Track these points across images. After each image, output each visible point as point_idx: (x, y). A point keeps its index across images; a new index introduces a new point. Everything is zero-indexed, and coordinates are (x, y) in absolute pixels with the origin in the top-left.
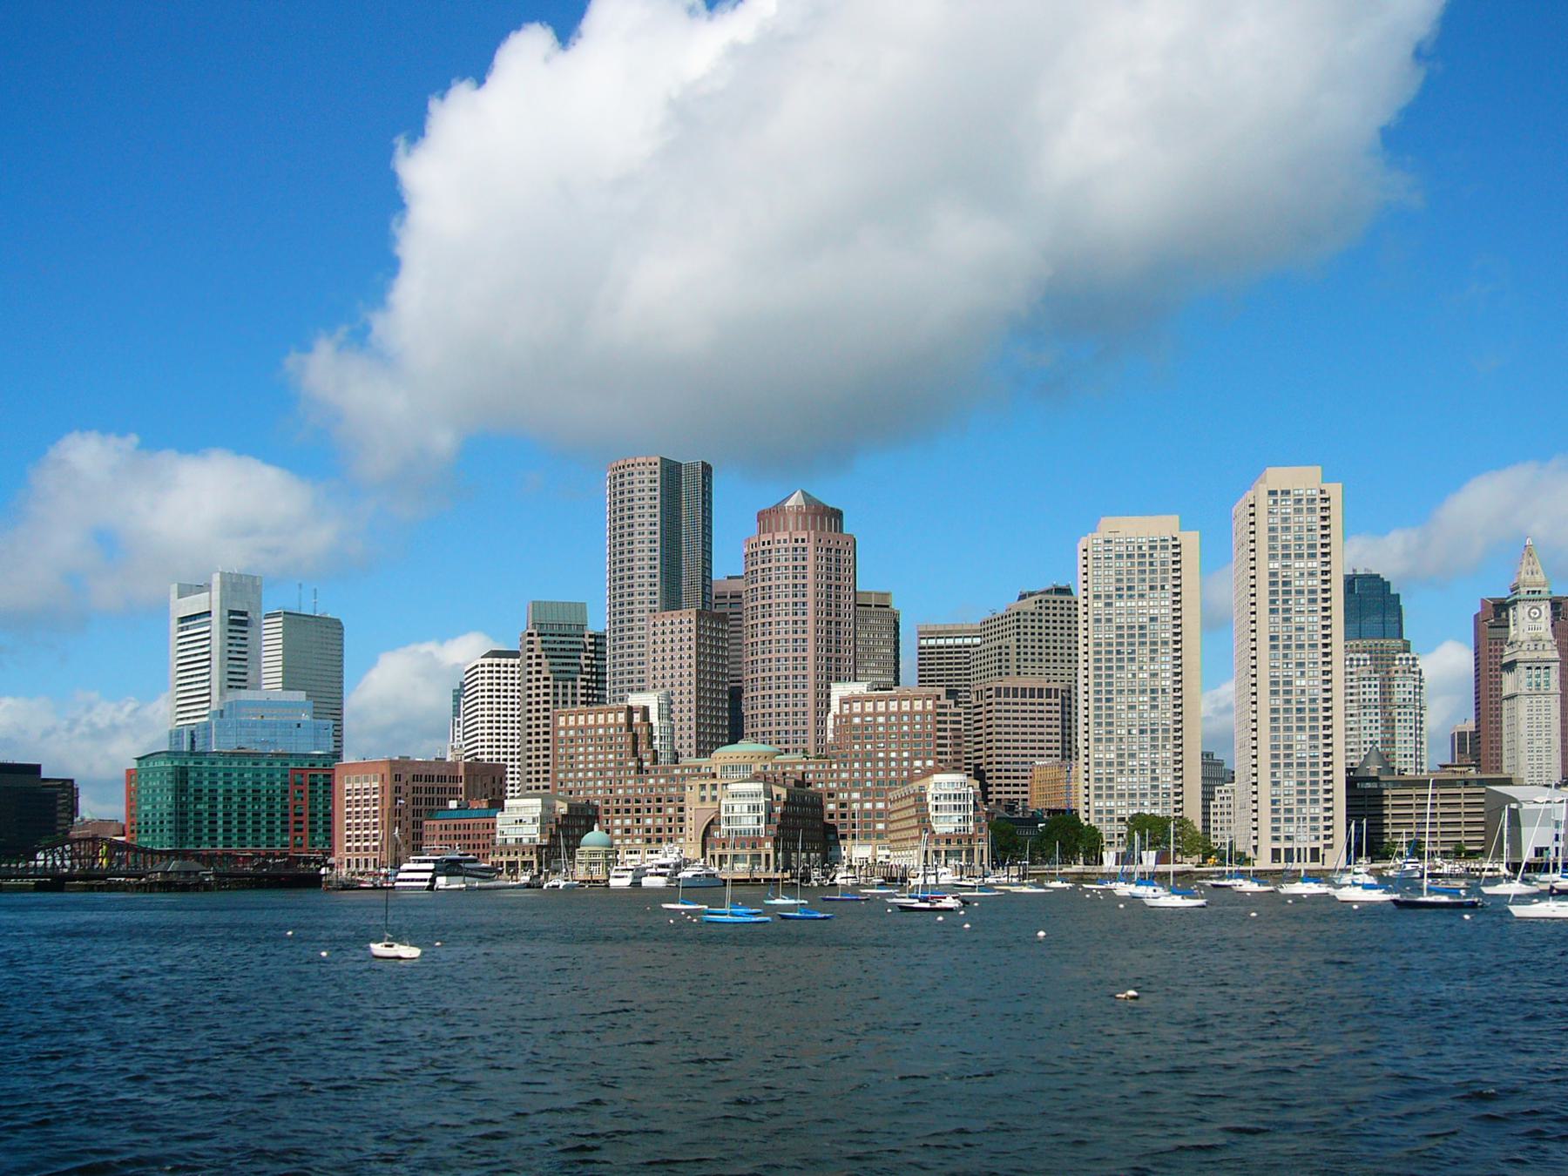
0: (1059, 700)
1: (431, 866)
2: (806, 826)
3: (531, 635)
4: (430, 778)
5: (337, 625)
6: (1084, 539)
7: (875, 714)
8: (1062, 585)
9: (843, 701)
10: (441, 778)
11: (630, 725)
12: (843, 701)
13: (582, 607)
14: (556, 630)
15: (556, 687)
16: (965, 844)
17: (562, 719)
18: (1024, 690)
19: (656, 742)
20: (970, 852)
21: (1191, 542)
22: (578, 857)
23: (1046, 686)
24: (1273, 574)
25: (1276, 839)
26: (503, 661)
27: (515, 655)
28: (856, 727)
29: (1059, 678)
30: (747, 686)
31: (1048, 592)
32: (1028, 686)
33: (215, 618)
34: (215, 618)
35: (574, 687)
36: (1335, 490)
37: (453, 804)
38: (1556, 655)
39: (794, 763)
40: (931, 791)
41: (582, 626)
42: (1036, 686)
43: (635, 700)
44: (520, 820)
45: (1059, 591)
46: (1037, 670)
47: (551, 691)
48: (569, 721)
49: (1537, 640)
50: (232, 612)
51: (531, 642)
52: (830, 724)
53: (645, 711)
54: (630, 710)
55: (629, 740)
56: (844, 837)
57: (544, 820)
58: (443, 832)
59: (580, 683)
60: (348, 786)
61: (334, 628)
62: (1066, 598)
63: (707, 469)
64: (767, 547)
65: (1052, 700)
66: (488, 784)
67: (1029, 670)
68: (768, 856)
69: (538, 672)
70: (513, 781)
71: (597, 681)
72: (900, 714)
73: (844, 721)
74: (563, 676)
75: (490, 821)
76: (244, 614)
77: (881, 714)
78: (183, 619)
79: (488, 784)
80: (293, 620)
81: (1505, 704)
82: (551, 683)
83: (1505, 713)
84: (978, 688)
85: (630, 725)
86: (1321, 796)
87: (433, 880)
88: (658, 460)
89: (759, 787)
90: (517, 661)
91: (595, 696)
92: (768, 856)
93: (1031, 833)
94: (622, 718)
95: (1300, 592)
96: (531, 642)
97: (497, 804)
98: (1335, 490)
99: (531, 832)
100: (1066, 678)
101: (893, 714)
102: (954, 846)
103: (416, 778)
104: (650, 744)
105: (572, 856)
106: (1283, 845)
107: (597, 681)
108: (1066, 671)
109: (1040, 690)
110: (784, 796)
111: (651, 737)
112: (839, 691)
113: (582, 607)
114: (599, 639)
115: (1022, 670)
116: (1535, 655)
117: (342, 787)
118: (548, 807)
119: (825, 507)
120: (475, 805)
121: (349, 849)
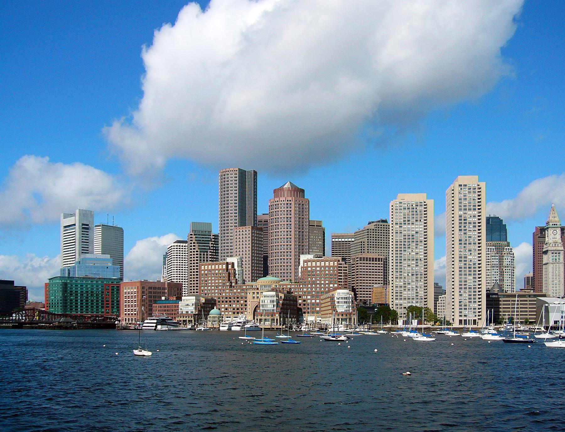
0: (382, 263)
1: (155, 321)
2: (291, 308)
3: (191, 235)
4: (155, 288)
5: (121, 229)
7: (316, 267)
8: (384, 219)
9: (305, 261)
10: (159, 288)
12: (305, 261)
14: (200, 233)
15: (201, 254)
16: (348, 316)
19: (237, 276)
20: (350, 319)
21: (431, 203)
22: (209, 319)
23: (378, 257)
25: (461, 316)
28: (309, 271)
31: (379, 222)
32: (371, 257)
33: (77, 226)
34: (77, 226)
35: (207, 255)
36: (483, 185)
37: (163, 298)
38: (562, 248)
40: (336, 296)
41: (210, 232)
43: (229, 260)
49: (555, 243)
50: (83, 224)
51: (191, 238)
54: (227, 264)
56: (305, 313)
57: (196, 305)
58: (160, 309)
61: (121, 230)
62: (385, 224)
63: (255, 173)
64: (277, 203)
66: (176, 291)
67: (372, 251)
68: (277, 319)
69: (194, 249)
70: (185, 290)
72: (325, 267)
73: (305, 269)
74: (203, 251)
75: (177, 305)
76: (88, 225)
78: (65, 227)
79: (176, 291)
80: (105, 228)
85: (227, 269)
87: (156, 327)
88: (237, 169)
89: (274, 293)
90: (187, 245)
91: (215, 258)
92: (277, 319)
93: (373, 312)
94: (224, 266)
95: (470, 223)
96: (191, 238)
97: (179, 298)
98: (483, 185)
99: (191, 309)
100: (385, 254)
101: (323, 267)
102: (344, 317)
103: (150, 288)
105: (206, 318)
106: (463, 318)
110: (283, 297)
112: (303, 258)
114: (216, 236)
115: (369, 251)
116: (555, 248)
117: (123, 291)
118: (198, 300)
120: (171, 298)
121: (126, 314)
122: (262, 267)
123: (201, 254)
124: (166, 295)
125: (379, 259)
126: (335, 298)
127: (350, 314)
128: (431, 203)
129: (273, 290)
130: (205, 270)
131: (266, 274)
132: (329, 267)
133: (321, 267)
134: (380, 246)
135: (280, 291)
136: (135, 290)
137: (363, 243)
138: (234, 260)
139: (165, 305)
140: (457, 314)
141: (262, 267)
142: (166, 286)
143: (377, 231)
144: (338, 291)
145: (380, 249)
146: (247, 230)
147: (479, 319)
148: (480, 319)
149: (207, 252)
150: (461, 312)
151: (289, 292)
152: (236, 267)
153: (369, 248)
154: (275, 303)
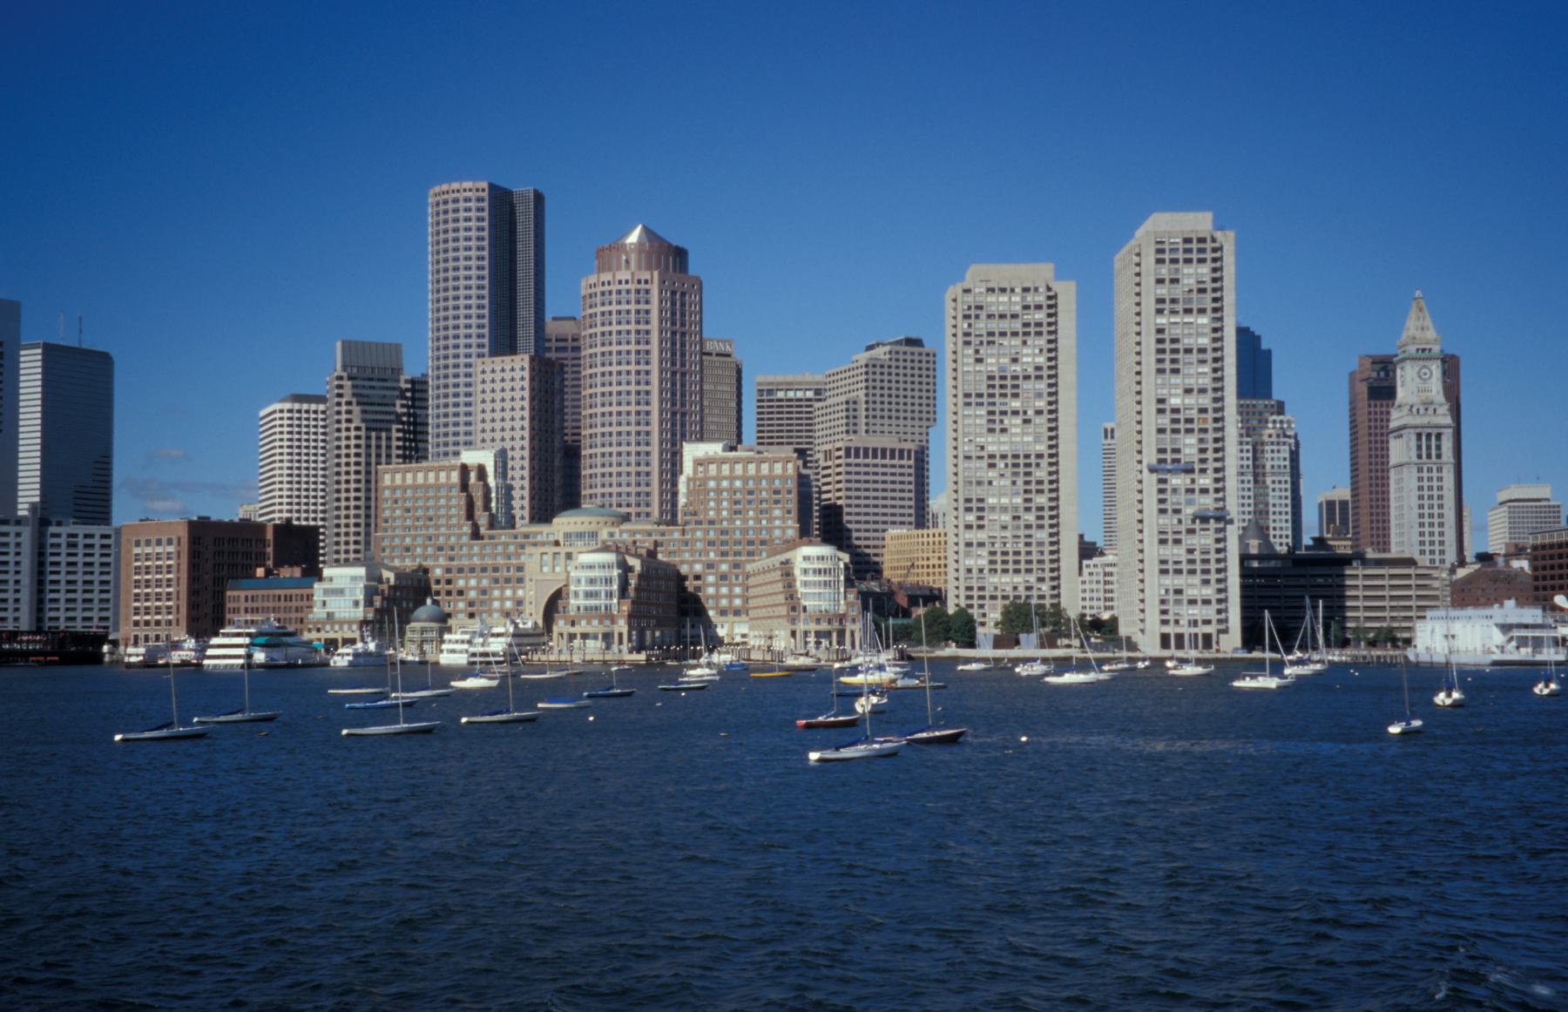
0: (912, 462)
1: (247, 640)
2: (669, 607)
3: (341, 378)
5: (104, 360)
6: (951, 288)
8: (914, 335)
9: (698, 463)
11: (464, 486)
12: (698, 463)
13: (396, 349)
14: (376, 375)
15: (368, 438)
16: (836, 625)
17: (387, 477)
18: (875, 450)
19: (493, 504)
20: (841, 633)
21: (1067, 294)
22: (409, 635)
23: (898, 446)
24: (1160, 331)
25: (1165, 622)
26: (305, 406)
27: (321, 399)
29: (909, 437)
30: (586, 442)
31: (898, 343)
32: (879, 446)
35: (389, 439)
36: (1228, 240)
37: (260, 572)
39: (641, 532)
40: (799, 565)
41: (398, 371)
42: (889, 446)
43: (470, 457)
44: (341, 592)
45: (910, 342)
46: (886, 428)
47: (362, 442)
48: (395, 477)
51: (340, 387)
52: (682, 488)
53: (481, 470)
54: (465, 469)
55: (463, 502)
57: (370, 593)
58: (249, 605)
59: (395, 435)
60: (137, 550)
61: (104, 360)
62: (916, 350)
63: (539, 198)
64: (607, 288)
65: (904, 462)
66: (300, 548)
67: (878, 428)
68: (621, 635)
69: (349, 421)
70: (326, 545)
71: (415, 432)
72: (758, 478)
73: (699, 486)
74: (375, 426)
75: (305, 592)
77: (725, 478)
79: (300, 548)
80: (54, 356)
81: (1393, 475)
82: (362, 433)
83: (1392, 482)
84: (827, 447)
85: (464, 486)
86: (1034, 549)
87: (249, 656)
88: (485, 185)
89: (610, 558)
90: (322, 407)
91: (414, 449)
92: (621, 635)
93: (896, 610)
94: (455, 477)
95: (1188, 351)
96: (340, 387)
97: (313, 573)
98: (1228, 240)
100: (917, 437)
101: (752, 478)
102: (824, 626)
104: (487, 507)
105: (402, 633)
106: (1170, 630)
107: (415, 432)
108: (917, 430)
109: (893, 451)
110: (638, 568)
111: (487, 499)
112: (692, 451)
113: (396, 349)
114: (418, 388)
115: (872, 428)
116: (1425, 420)
117: (129, 551)
118: (374, 577)
119: (670, 245)
120: (286, 572)
121: (136, 623)
122: (557, 481)
123: (368, 438)
124: (270, 563)
125: (902, 451)
126: (797, 572)
127: (842, 618)
128: (1067, 294)
129: (605, 549)
130: (394, 489)
131: (571, 501)
132: (771, 478)
133: (745, 479)
134: (902, 414)
135: (628, 552)
136: (171, 549)
137: (851, 406)
138: (483, 457)
139: (288, 592)
140: (1153, 617)
141: (557, 481)
142: (270, 535)
143: (894, 371)
144: (893, 531)
145: (901, 422)
146: (516, 370)
147: (1219, 632)
148: (1226, 631)
149: (389, 430)
150: (1164, 612)
151: (652, 554)
152: (491, 481)
153: (871, 420)
154: (615, 587)
